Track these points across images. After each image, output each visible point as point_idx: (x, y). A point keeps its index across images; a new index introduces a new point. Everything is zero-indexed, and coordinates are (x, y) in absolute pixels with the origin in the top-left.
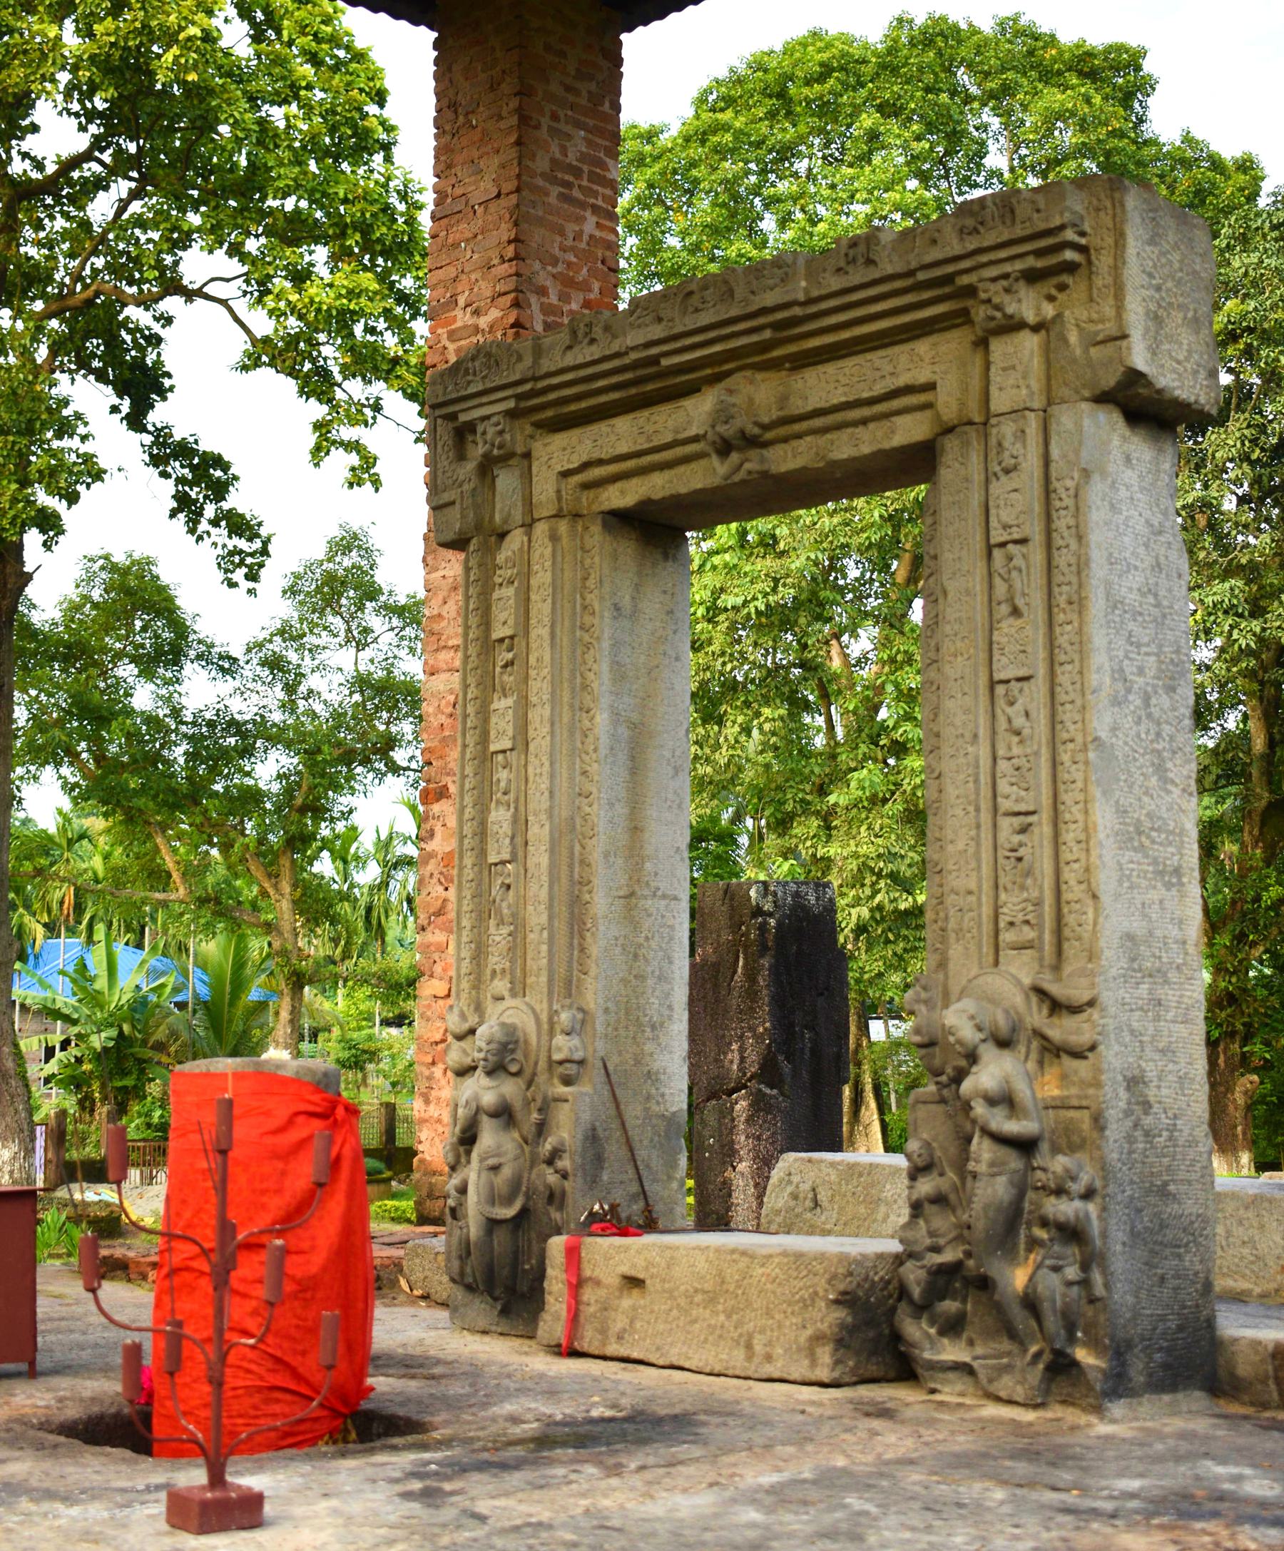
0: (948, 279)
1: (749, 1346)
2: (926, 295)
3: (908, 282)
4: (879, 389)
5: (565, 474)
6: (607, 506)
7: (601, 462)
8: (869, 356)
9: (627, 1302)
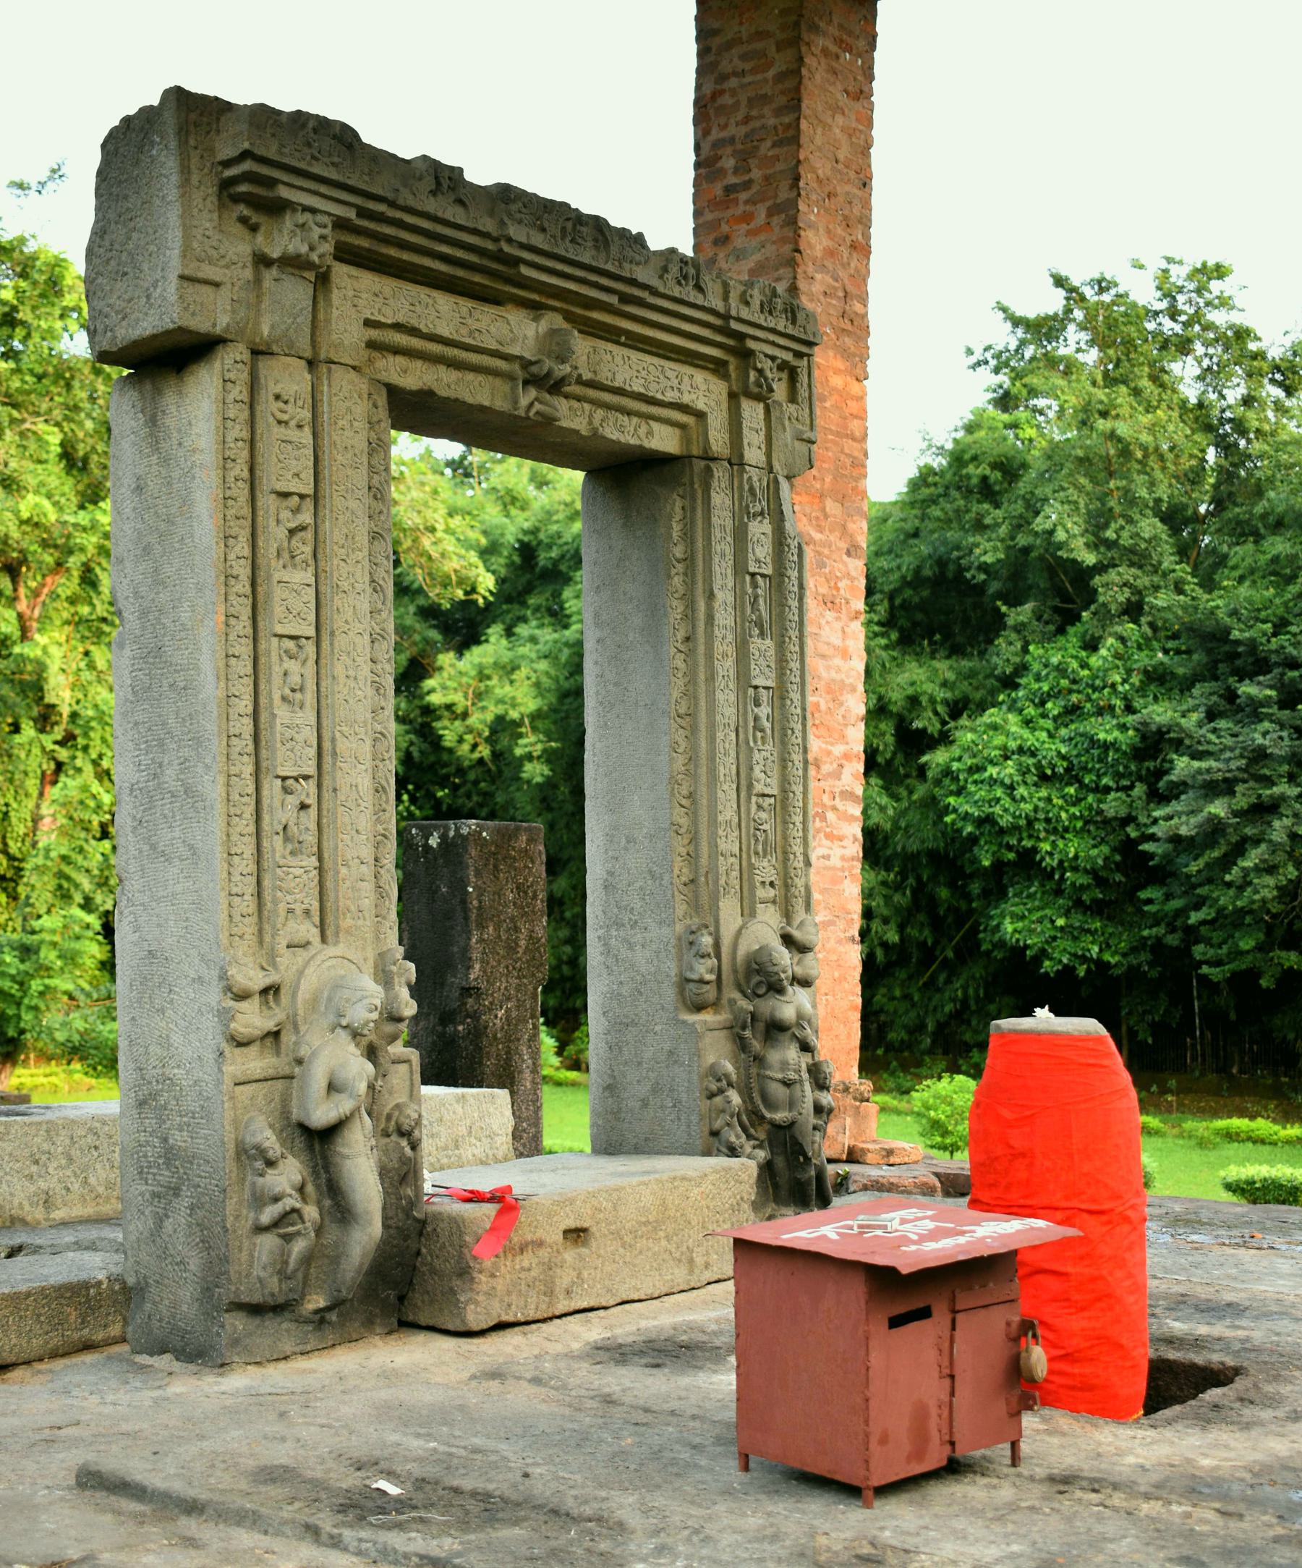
0: (741, 337)
1: (691, 1261)
2: (719, 338)
3: (718, 322)
4: (670, 396)
5: (368, 323)
6: (384, 377)
7: (414, 332)
8: (435, 293)
9: (570, 1255)
